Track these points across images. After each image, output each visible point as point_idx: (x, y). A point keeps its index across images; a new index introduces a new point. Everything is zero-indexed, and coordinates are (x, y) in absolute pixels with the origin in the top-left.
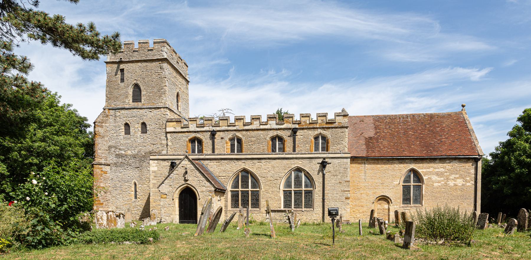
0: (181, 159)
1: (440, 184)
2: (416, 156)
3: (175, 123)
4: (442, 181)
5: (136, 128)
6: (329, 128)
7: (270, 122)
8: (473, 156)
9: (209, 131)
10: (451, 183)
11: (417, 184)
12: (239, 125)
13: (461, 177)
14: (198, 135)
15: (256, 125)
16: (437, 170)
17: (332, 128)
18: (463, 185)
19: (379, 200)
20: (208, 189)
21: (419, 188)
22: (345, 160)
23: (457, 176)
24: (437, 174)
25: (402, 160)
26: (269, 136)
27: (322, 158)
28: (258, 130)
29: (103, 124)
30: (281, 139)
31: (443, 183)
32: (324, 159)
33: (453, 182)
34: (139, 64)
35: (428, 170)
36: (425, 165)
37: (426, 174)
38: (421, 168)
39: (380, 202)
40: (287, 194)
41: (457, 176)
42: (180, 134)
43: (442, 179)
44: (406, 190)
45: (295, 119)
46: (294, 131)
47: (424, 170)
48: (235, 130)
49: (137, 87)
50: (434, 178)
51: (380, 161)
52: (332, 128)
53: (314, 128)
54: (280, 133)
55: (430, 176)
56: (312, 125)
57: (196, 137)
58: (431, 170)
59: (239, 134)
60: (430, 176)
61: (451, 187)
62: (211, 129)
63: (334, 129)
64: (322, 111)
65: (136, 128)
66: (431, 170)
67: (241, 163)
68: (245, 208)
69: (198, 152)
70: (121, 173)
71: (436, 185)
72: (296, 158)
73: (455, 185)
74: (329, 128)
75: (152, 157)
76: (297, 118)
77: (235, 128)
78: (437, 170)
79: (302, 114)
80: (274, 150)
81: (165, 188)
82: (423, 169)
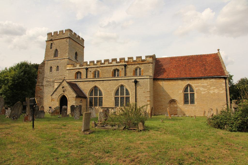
0: (60, 82)
1: (205, 92)
2: (216, 76)
3: (70, 65)
4: (206, 91)
5: (54, 69)
6: (142, 64)
7: (113, 62)
8: (221, 76)
9: (85, 68)
10: (212, 92)
11: (191, 93)
12: (99, 65)
13: (217, 88)
14: (79, 70)
15: (106, 64)
16: (203, 85)
17: (144, 63)
18: (218, 93)
19: (170, 103)
20: (73, 96)
21: (192, 95)
22: (147, 80)
23: (215, 88)
24: (203, 87)
25: (182, 79)
26: (113, 69)
27: (134, 79)
28: (107, 66)
29: (42, 68)
30: (80, 73)
31: (207, 91)
32: (135, 79)
33: (213, 91)
34: (58, 40)
35: (197, 85)
36: (196, 81)
37: (196, 87)
38: (194, 84)
39: (171, 103)
40: (116, 99)
41: (215, 88)
42: (72, 70)
43: (206, 89)
44: (186, 96)
45: (143, 59)
46: (125, 66)
47: (196, 85)
48: (96, 67)
49: (56, 50)
50: (202, 89)
51: (171, 80)
52: (144, 63)
53: (134, 64)
54: (117, 67)
55: (199, 88)
56: (135, 63)
57: (79, 71)
58: (199, 84)
59: (98, 69)
60: (199, 88)
61: (212, 94)
62: (86, 67)
63: (145, 64)
64: (139, 55)
65: (54, 69)
66: (199, 84)
67: (94, 83)
68: (152, 109)
69: (80, 78)
70: (47, 89)
71: (203, 93)
72: (121, 80)
73: (214, 93)
74: (142, 64)
75: (55, 81)
76: (126, 60)
77: (96, 66)
78: (203, 85)
79: (129, 57)
80: (95, 77)
81: (54, 96)
82: (194, 84)
